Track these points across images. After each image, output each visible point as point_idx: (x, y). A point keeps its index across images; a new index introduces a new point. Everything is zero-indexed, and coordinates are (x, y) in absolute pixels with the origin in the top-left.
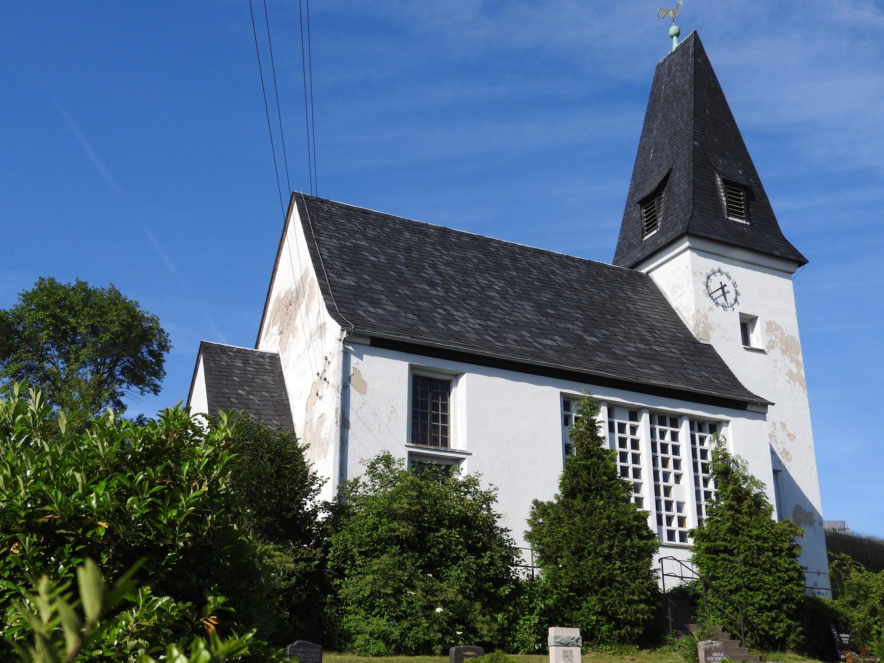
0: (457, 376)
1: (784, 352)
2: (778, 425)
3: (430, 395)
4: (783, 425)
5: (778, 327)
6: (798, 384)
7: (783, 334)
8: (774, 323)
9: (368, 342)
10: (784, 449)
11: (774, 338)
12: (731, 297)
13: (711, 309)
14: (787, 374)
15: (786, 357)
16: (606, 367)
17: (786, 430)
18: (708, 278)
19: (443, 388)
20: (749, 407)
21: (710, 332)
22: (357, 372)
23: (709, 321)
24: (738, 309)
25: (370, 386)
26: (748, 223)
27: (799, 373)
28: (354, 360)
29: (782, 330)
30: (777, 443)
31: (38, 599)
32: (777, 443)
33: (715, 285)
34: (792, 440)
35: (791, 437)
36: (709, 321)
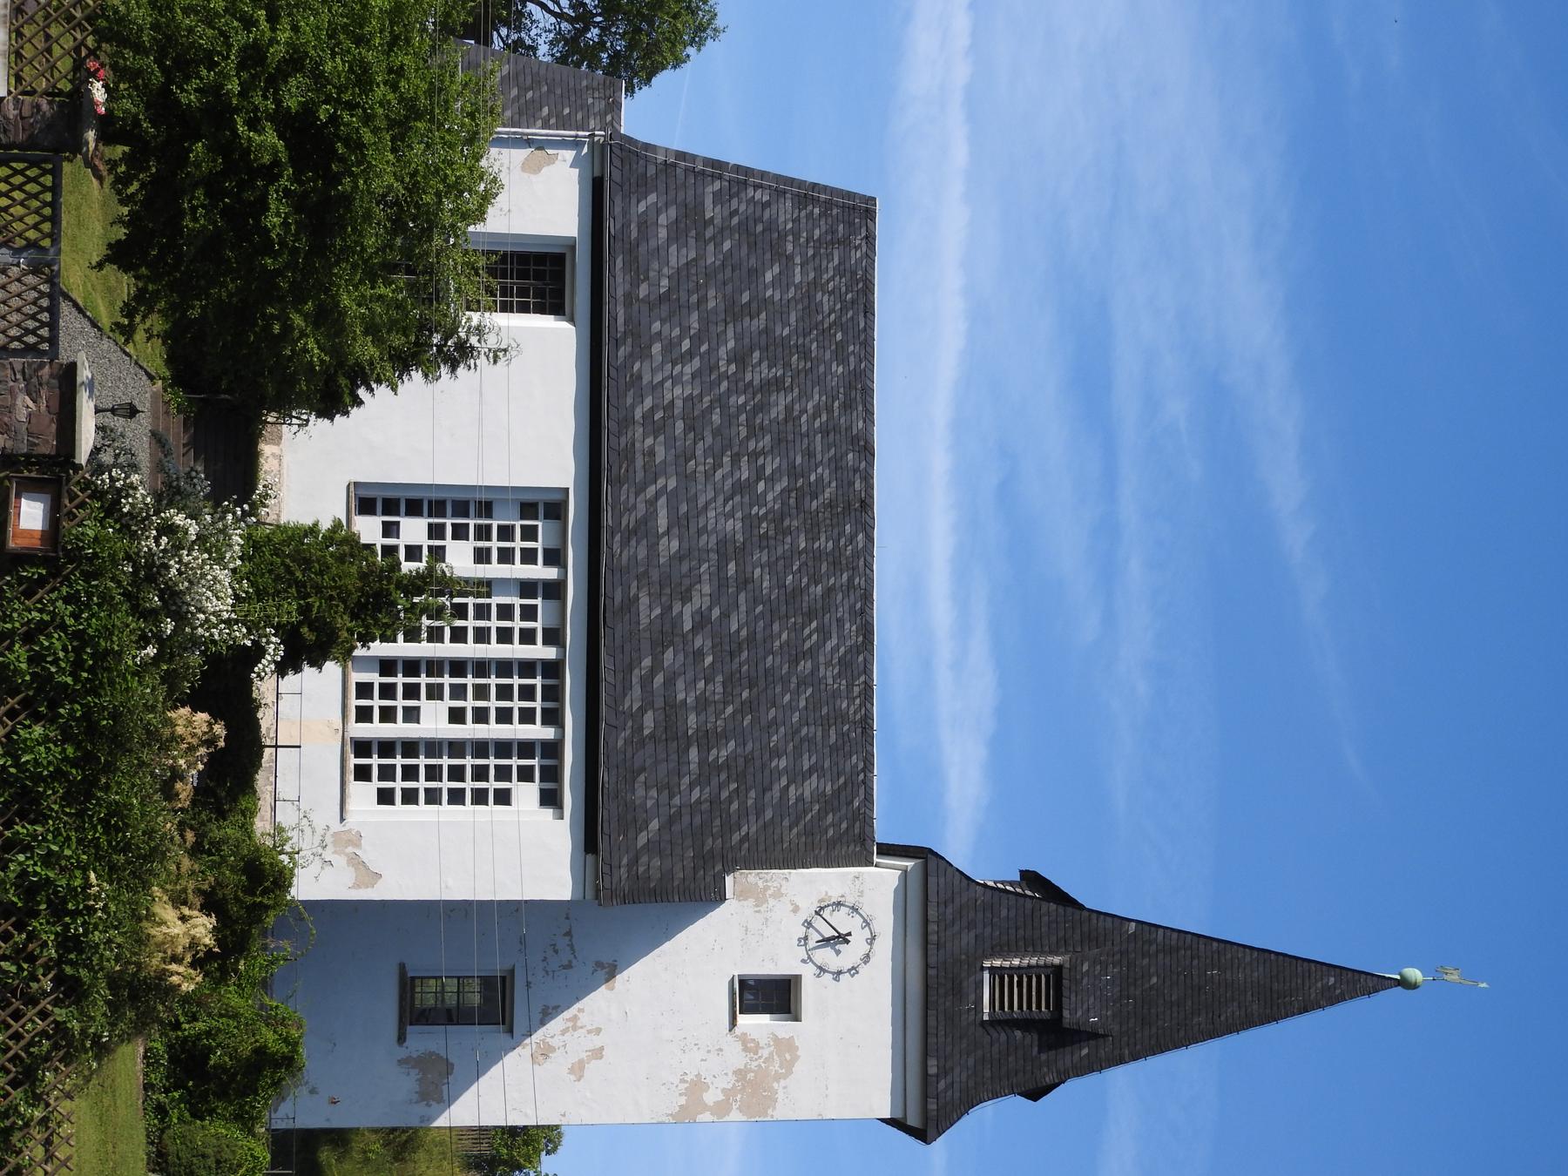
0: (572, 320)
1: (740, 1074)
2: (597, 1041)
3: (540, 284)
4: (598, 1053)
5: (788, 1066)
6: (683, 1100)
7: (778, 1077)
8: (795, 1058)
9: (597, 174)
10: (552, 1049)
11: (765, 1053)
12: (825, 956)
13: (796, 909)
14: (698, 1075)
15: (732, 1078)
16: (610, 548)
17: (590, 1059)
18: (854, 909)
19: (553, 304)
20: (590, 857)
21: (751, 902)
22: (552, 160)
23: (771, 902)
24: (807, 973)
25: (533, 177)
26: (986, 1018)
27: (705, 1108)
28: (569, 155)
29: (785, 1077)
30: (563, 1032)
31: (132, 424)
32: (563, 1032)
33: (843, 921)
34: (571, 1071)
35: (578, 1070)
36: (771, 902)
